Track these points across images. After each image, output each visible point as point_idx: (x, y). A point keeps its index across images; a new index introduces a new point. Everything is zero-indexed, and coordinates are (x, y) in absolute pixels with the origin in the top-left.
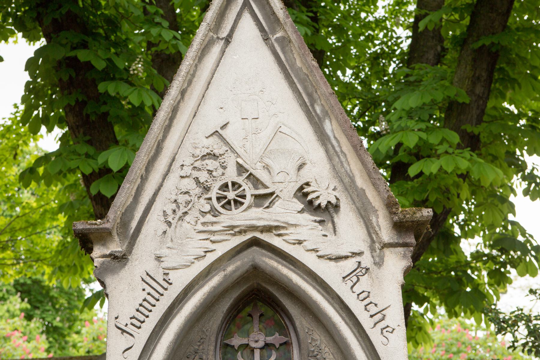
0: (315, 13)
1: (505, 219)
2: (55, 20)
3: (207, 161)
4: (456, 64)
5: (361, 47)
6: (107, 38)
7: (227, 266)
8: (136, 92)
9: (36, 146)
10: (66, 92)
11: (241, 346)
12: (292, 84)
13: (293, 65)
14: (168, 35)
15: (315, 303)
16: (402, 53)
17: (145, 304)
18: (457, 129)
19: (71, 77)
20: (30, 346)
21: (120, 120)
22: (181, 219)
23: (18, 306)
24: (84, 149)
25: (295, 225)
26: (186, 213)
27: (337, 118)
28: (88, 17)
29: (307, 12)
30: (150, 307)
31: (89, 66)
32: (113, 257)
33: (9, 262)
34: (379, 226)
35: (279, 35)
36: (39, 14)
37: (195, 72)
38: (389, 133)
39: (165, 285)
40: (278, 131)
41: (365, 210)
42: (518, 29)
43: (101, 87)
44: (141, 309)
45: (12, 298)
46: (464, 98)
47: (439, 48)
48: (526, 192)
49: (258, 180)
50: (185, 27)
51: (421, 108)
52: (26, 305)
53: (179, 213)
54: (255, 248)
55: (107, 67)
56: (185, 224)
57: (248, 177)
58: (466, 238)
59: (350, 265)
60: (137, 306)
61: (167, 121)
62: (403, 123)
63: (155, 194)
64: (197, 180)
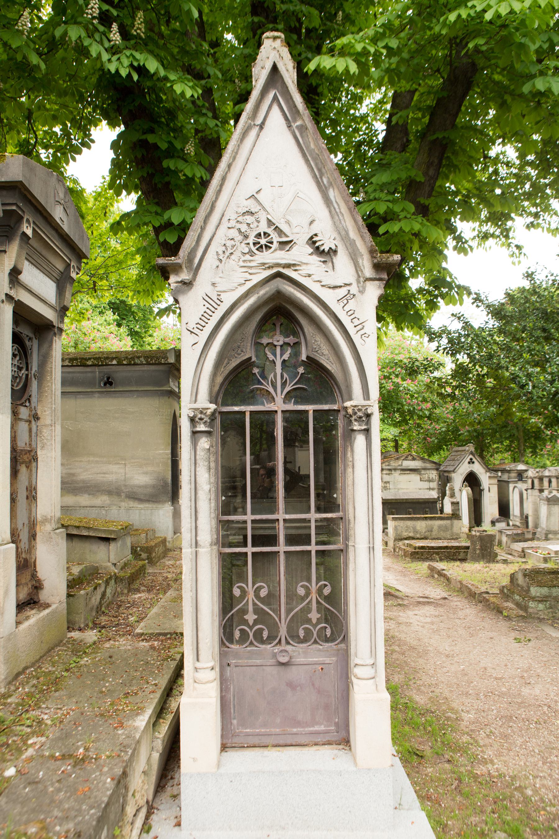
0: (317, 109)
1: (440, 266)
2: (130, 111)
3: (246, 217)
4: (416, 152)
5: (349, 137)
6: (168, 125)
7: (260, 291)
8: (189, 167)
9: (118, 207)
10: (140, 166)
11: (268, 344)
12: (307, 161)
13: (308, 147)
14: (212, 123)
15: (318, 317)
16: (378, 142)
17: (205, 315)
18: (413, 202)
19: (143, 155)
20: (121, 344)
21: (178, 187)
22: (228, 257)
23: (112, 318)
24: (154, 208)
25: (307, 264)
26: (232, 253)
27: (338, 188)
28: (154, 109)
29: (312, 107)
30: (209, 317)
31: (156, 146)
32: (183, 283)
33: (106, 288)
34: (363, 266)
35: (299, 123)
36: (118, 106)
37: (238, 150)
38: (364, 201)
39: (219, 302)
40: (296, 196)
41: (355, 255)
42: (462, 127)
43: (165, 164)
44: (203, 318)
45: (107, 312)
46: (421, 178)
47: (405, 140)
48: (455, 248)
49: (281, 231)
50: (221, 118)
51: (390, 184)
52: (116, 317)
53: (227, 254)
54: (279, 279)
55: (168, 148)
56: (231, 261)
57: (275, 229)
58: (412, 278)
59: (343, 292)
60: (200, 316)
61: (219, 187)
62: (377, 195)
63: (211, 240)
64: (239, 230)
